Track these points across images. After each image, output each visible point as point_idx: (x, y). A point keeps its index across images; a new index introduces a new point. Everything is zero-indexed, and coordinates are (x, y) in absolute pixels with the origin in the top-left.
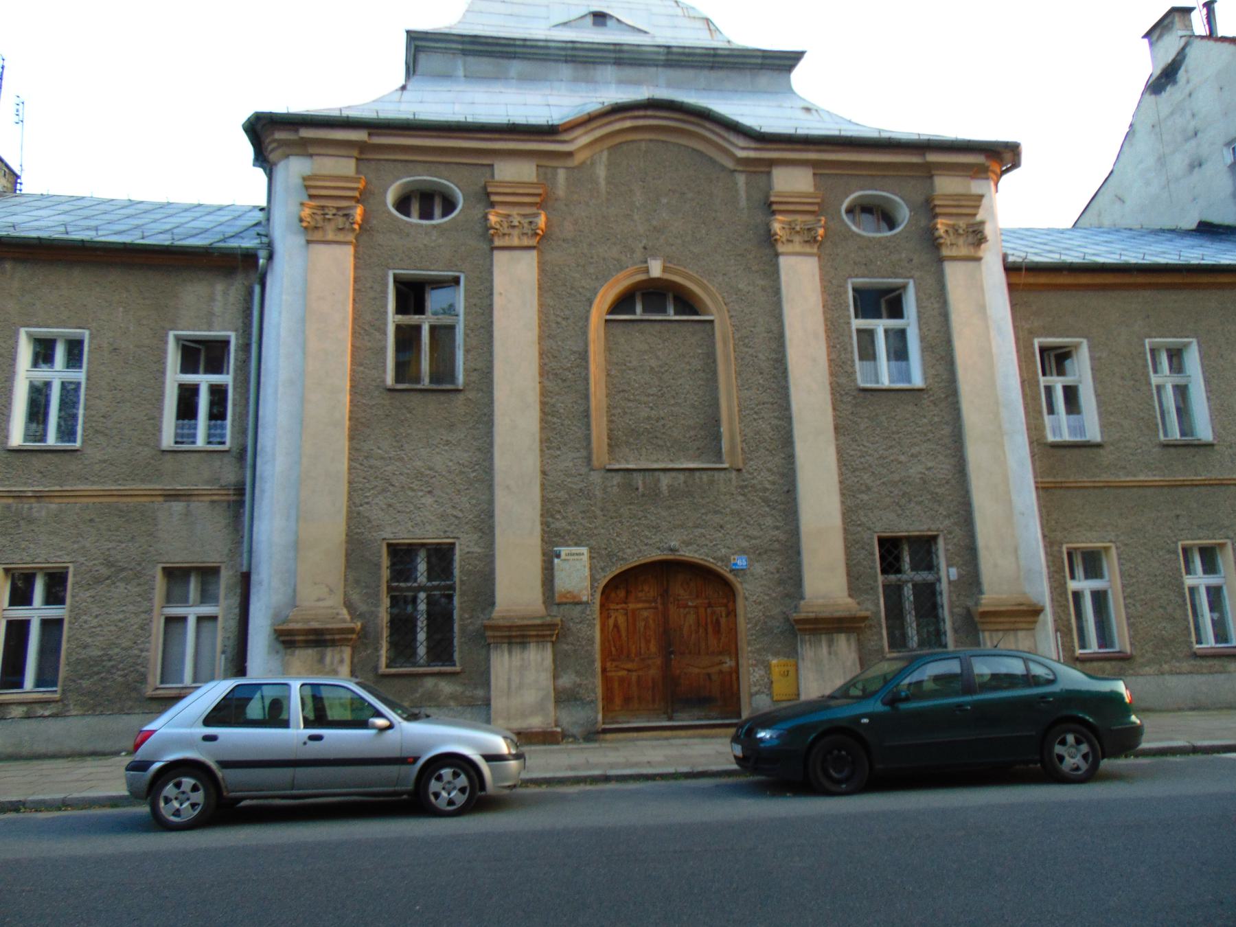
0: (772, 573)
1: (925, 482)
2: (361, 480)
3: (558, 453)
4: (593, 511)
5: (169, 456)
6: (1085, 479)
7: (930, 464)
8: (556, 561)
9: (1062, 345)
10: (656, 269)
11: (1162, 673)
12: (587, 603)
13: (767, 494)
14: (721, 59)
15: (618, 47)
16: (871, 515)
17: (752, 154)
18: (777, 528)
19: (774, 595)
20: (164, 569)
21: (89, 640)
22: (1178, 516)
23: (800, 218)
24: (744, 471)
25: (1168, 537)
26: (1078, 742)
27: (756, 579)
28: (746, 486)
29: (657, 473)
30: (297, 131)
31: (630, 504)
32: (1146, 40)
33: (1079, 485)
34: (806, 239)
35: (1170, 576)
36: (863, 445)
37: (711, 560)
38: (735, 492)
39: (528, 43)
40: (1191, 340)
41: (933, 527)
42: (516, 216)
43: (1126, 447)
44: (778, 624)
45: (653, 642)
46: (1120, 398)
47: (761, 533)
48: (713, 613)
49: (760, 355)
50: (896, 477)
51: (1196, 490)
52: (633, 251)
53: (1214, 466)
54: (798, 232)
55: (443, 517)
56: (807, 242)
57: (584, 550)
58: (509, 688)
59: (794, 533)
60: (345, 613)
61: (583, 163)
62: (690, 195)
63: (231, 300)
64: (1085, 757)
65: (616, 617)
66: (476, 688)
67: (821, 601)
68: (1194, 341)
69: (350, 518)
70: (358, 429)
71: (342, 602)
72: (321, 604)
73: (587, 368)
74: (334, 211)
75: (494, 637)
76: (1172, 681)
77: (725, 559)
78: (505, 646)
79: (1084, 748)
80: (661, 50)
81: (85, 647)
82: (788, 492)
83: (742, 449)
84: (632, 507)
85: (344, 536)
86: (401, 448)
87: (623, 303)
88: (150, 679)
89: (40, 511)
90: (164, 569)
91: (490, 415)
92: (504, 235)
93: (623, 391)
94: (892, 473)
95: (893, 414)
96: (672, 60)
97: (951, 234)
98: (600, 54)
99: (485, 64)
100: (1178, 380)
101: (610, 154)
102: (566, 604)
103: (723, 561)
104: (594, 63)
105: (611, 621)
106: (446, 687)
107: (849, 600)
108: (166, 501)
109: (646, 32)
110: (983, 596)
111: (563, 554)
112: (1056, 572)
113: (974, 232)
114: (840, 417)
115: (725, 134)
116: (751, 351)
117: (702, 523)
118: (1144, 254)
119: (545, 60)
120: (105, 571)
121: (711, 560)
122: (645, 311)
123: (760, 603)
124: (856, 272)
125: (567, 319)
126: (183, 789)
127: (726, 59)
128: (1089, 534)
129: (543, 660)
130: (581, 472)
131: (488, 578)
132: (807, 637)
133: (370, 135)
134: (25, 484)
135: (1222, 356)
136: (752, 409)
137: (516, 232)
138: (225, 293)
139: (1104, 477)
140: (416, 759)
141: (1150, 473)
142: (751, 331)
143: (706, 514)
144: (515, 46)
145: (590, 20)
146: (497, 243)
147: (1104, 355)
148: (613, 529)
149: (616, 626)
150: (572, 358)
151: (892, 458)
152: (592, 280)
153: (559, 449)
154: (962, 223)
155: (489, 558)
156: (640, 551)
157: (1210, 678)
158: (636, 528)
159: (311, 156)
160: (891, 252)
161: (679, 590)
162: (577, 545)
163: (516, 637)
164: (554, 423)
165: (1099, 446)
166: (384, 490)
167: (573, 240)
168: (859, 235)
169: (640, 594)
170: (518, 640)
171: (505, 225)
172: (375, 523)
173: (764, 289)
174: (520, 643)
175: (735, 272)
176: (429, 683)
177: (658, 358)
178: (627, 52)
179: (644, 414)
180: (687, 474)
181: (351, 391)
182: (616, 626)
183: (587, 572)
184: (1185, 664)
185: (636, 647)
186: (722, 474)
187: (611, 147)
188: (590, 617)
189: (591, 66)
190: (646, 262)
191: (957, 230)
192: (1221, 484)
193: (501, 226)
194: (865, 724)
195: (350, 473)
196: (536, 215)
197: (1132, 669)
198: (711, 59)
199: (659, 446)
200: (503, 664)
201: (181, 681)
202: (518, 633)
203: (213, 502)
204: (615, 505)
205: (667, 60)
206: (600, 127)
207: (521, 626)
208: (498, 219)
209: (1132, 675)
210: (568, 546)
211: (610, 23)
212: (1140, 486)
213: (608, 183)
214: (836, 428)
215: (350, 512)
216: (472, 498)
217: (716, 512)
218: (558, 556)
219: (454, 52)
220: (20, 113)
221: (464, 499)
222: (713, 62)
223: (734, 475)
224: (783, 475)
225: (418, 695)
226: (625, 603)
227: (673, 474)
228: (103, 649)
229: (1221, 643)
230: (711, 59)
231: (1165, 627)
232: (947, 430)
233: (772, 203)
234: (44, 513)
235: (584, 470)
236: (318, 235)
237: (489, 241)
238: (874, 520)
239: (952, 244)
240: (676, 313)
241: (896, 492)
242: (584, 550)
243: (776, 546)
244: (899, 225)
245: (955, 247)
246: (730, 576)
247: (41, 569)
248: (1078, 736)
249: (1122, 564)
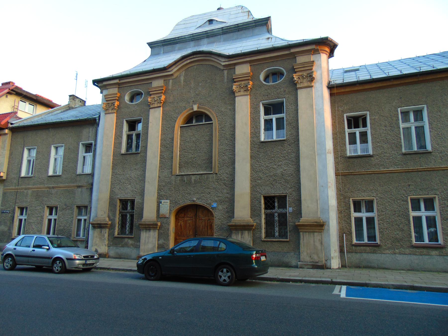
0: (225, 209)
1: (283, 175)
2: (114, 181)
3: (164, 170)
4: (172, 189)
5: (78, 176)
6: (363, 171)
7: (285, 168)
8: (160, 204)
9: (363, 115)
10: (195, 108)
11: (395, 254)
12: (168, 218)
13: (225, 182)
14: (241, 27)
15: (206, 32)
16: (261, 188)
17: (227, 63)
18: (228, 193)
19: (225, 216)
21: (61, 225)
22: (409, 185)
23: (243, 82)
24: (218, 174)
25: (403, 194)
26: (227, 272)
27: (220, 211)
28: (218, 179)
29: (191, 176)
30: (103, 83)
31: (182, 186)
33: (360, 173)
34: (245, 90)
35: (402, 212)
36: (261, 163)
37: (205, 204)
38: (214, 181)
39: (179, 38)
41: (284, 192)
42: (156, 97)
43: (384, 156)
44: (226, 227)
45: (191, 231)
46: (383, 135)
47: (222, 195)
48: (210, 222)
49: (227, 133)
50: (272, 174)
51: (420, 173)
52: (189, 103)
53: (431, 162)
54: (242, 88)
55: (132, 191)
56: (245, 91)
57: (168, 201)
58: (145, 243)
59: (233, 195)
60: (107, 219)
61: (177, 76)
62: (209, 81)
63: (93, 132)
64: (229, 277)
65: (181, 222)
66: (137, 242)
67: (239, 219)
69: (111, 192)
70: (114, 166)
71: (107, 216)
72: (102, 216)
73: (173, 143)
74: (111, 104)
75: (142, 227)
76: (399, 257)
77: (210, 204)
78: (145, 230)
79: (229, 274)
80: (220, 29)
81: (60, 226)
82: (232, 180)
83: (218, 166)
84: (183, 187)
85: (109, 197)
86: (124, 171)
87: (189, 120)
88: (72, 235)
89: (54, 191)
91: (146, 160)
92: (153, 104)
93: (185, 149)
94: (270, 172)
95: (273, 150)
96: (224, 32)
97: (301, 78)
98: (201, 36)
99: (166, 48)
100: (419, 124)
101: (185, 72)
102: (162, 218)
103: (209, 205)
104: (201, 39)
105: (179, 224)
106: (130, 242)
109: (225, 22)
111: (162, 202)
112: (346, 209)
113: (310, 76)
114: (253, 153)
116: (224, 132)
117: (204, 192)
118: (388, 72)
119: (216, 36)
120: (65, 207)
121: (205, 204)
122: (196, 122)
123: (220, 219)
124: (263, 99)
125: (169, 128)
126: (57, 264)
128: (363, 194)
129: (154, 235)
130: (169, 176)
131: (142, 209)
132: (234, 231)
133: (120, 80)
134: (51, 185)
135: (440, 111)
136: (223, 152)
137: (156, 102)
138: (92, 131)
139: (373, 170)
140: (52, 258)
141: (395, 167)
142: (225, 125)
143: (205, 189)
144: (176, 40)
145: (208, 23)
146: (151, 107)
147: (377, 117)
148: (177, 194)
149: (181, 225)
150: (170, 140)
151: (271, 167)
152: (177, 114)
153: (164, 169)
154: (305, 74)
155: (142, 204)
156: (184, 201)
157: (421, 257)
158: (184, 194)
159: (107, 89)
160: (277, 89)
161: (200, 214)
162: (167, 199)
163: (147, 227)
164: (163, 161)
165: (430, 153)
166: (119, 184)
167: (172, 102)
168: (266, 85)
169: (188, 215)
170: (148, 229)
171: (153, 101)
172: (116, 193)
173: (230, 110)
174: (149, 229)
175: (221, 105)
176: (126, 240)
177: (195, 137)
178: (210, 33)
179: (190, 156)
180: (200, 175)
181: (113, 155)
182: (181, 225)
183: (169, 207)
184: (407, 250)
185: (186, 232)
186: (211, 175)
187: (185, 70)
188: (168, 222)
189: (200, 40)
190: (193, 106)
191: (303, 77)
192: (433, 170)
193: (152, 101)
194: (160, 259)
195: (111, 179)
196: (161, 96)
197: (380, 251)
198: (237, 28)
199: (194, 167)
200: (144, 235)
201: (80, 236)
202: (148, 226)
203: (87, 188)
204: (178, 187)
205: (223, 32)
206: (180, 64)
207: (149, 224)
208: (151, 99)
209: (380, 253)
210: (164, 200)
211: (214, 22)
212: (79, 187)
213: (184, 82)
214: (251, 157)
215: (111, 190)
216: (140, 185)
217: (208, 188)
218: (161, 203)
219: (160, 46)
220: (86, 84)
221: (138, 186)
223: (215, 175)
224: (231, 175)
225: (123, 243)
226: (184, 218)
227: (196, 176)
228: (63, 227)
229: (358, 241)
230: (237, 28)
231: (398, 234)
232: (293, 155)
233: (234, 79)
234: (54, 192)
235: (170, 176)
236: (107, 112)
237: (149, 106)
238: (262, 190)
239: (301, 82)
240: (196, 122)
241: (271, 179)
242: (168, 201)
243: (227, 199)
245: (302, 83)
246: (211, 210)
247: (55, 206)
248: (227, 269)
249: (378, 206)
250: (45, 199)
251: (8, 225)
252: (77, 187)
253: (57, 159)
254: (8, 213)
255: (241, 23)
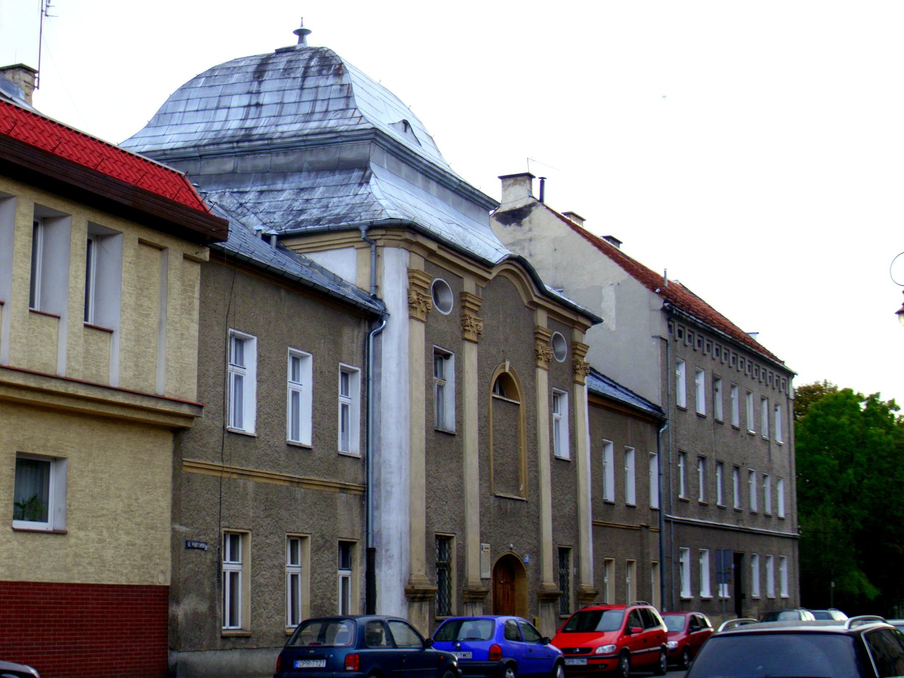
20: (340, 542)
32: (500, 181)
39: (417, 157)
40: (308, 354)
68: (255, 338)
89: (299, 492)
90: (340, 542)
107: (554, 584)
108: (340, 492)
109: (420, 145)
110: (582, 585)
115: (533, 285)
119: (445, 187)
127: (476, 198)
203: (355, 495)
205: (456, 188)
222: (440, 180)
244: (451, 304)
250: (284, 513)
251: (208, 590)
252: (340, 488)
253: (294, 390)
254: (203, 549)
255: (456, 178)
